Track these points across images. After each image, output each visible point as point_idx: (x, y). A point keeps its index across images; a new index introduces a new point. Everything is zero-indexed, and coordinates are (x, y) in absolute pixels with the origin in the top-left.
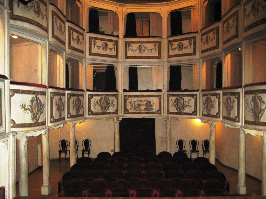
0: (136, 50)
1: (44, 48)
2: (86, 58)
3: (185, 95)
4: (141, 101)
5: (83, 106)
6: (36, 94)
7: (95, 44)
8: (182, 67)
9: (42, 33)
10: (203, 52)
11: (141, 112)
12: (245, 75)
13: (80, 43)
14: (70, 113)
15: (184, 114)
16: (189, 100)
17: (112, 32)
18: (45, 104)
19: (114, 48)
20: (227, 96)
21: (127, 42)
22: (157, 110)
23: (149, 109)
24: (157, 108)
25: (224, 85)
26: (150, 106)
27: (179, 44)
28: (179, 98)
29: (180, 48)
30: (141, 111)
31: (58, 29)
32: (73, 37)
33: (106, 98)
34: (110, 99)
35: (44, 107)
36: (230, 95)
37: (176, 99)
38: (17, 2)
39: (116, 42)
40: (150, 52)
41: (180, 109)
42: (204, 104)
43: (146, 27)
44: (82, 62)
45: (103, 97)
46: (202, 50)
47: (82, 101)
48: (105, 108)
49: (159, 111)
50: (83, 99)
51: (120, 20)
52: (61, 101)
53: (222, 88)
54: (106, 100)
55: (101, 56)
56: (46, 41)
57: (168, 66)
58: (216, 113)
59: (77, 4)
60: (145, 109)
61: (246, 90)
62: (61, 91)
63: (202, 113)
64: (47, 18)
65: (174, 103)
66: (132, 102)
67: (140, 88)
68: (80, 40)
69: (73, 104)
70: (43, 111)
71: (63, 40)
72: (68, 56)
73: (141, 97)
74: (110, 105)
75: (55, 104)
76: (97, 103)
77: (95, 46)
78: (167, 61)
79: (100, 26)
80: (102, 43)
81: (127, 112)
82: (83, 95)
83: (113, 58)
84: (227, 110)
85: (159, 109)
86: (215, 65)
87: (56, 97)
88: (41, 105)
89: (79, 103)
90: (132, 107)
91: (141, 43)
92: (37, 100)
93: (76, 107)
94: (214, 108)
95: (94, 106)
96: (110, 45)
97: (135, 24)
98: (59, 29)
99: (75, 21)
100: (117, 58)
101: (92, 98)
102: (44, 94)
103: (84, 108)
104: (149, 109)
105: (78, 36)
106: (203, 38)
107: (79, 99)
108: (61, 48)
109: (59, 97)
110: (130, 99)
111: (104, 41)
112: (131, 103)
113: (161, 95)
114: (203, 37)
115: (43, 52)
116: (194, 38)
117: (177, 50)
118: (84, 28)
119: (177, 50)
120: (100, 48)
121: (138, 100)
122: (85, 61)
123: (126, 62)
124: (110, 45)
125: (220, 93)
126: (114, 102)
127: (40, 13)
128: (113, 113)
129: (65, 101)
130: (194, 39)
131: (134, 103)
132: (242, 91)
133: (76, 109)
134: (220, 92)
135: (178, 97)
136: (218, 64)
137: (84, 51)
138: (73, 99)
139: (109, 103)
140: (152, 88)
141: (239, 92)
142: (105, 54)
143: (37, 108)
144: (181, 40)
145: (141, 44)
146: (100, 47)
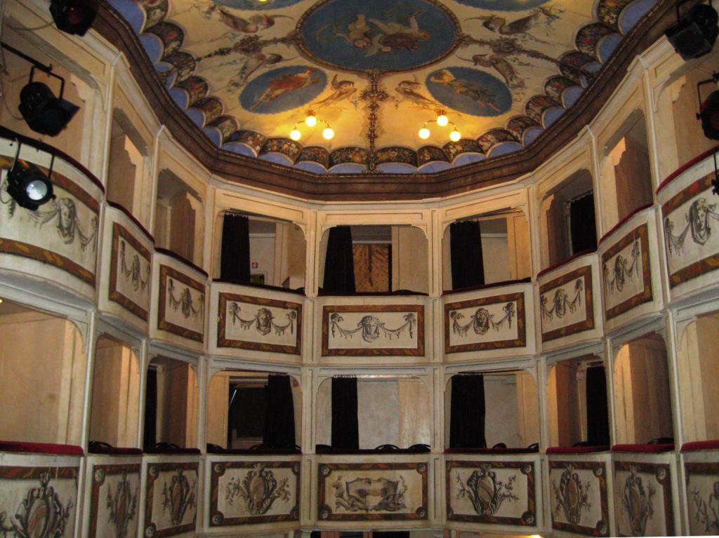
0: (356, 330)
1: (80, 333)
2: (208, 356)
3: (499, 463)
4: (369, 481)
5: (195, 500)
6: (44, 477)
7: (235, 314)
8: (485, 378)
9: (78, 290)
10: (547, 337)
11: (368, 515)
12: (683, 412)
13: (191, 313)
14: (154, 525)
15: (496, 520)
16: (511, 480)
17: (285, 278)
18: (71, 505)
19: (290, 326)
20: (630, 474)
21: (328, 309)
22: (417, 507)
23: (392, 505)
24: (416, 503)
25: (616, 439)
26: (394, 496)
27: (477, 313)
28: (480, 474)
29: (479, 324)
30: (370, 512)
31: (128, 276)
32: (172, 297)
33: (264, 474)
34: (275, 477)
35: (67, 515)
36: (639, 471)
37: (472, 476)
38: (10, 203)
39: (296, 309)
40: (394, 336)
41: (484, 506)
42: (557, 493)
43: (381, 260)
44: (195, 367)
45: (257, 469)
46: (544, 332)
47: (191, 484)
48: (260, 505)
49: (422, 513)
50: (195, 477)
51: (308, 246)
52: (124, 490)
53: (611, 447)
54: (264, 479)
55: (253, 349)
56: (91, 310)
57: (424, 225)
58: (596, 522)
59: (188, 201)
60: (381, 506)
61: (690, 461)
62: (128, 460)
63: (553, 519)
64: (95, 246)
65: (467, 488)
66: (341, 485)
67: (367, 439)
68: (193, 305)
69: (164, 495)
70: (63, 531)
71: (142, 305)
72: (155, 352)
73: (368, 469)
74: (277, 495)
75: (106, 502)
76: (237, 487)
77: (234, 319)
78: (445, 363)
79: (252, 260)
80: (256, 312)
81: (325, 515)
82: (194, 467)
83: (288, 353)
84: (632, 515)
85: (421, 505)
86: (583, 371)
87: (108, 479)
88: (58, 510)
89: (182, 491)
90: (341, 500)
91: (369, 312)
92: (45, 497)
93: (173, 505)
94: (589, 506)
95: (227, 498)
96: (280, 317)
97: (352, 251)
98: (131, 276)
99: (182, 252)
100: (300, 354)
101: (222, 473)
102: (69, 474)
103: (196, 506)
104: (392, 505)
105: (187, 293)
106: (546, 299)
107: (181, 479)
108: (134, 330)
109: (119, 478)
110: (336, 474)
111: (264, 304)
112: (337, 488)
113: (426, 464)
114: (546, 295)
115: (79, 343)
116: (521, 297)
117: (471, 330)
118: (206, 268)
119: (471, 330)
120: (251, 327)
121: (360, 477)
122: (205, 362)
123: (325, 367)
124: (280, 317)
125: (603, 461)
126: (288, 486)
127: (76, 231)
128: (286, 518)
129: (138, 488)
130: (521, 299)
131: (348, 489)
132: (678, 462)
133: (173, 511)
134: (606, 458)
135: (477, 469)
136: (589, 371)
137: (203, 335)
138: (165, 479)
139: (273, 489)
140: (400, 440)
141: (668, 463)
142: (263, 342)
143: (43, 521)
144: (482, 302)
145: (369, 314)
146: (251, 322)
